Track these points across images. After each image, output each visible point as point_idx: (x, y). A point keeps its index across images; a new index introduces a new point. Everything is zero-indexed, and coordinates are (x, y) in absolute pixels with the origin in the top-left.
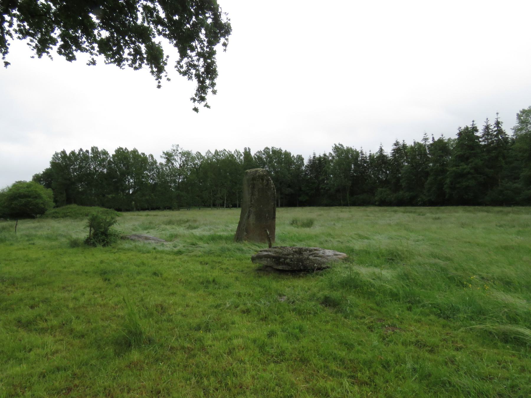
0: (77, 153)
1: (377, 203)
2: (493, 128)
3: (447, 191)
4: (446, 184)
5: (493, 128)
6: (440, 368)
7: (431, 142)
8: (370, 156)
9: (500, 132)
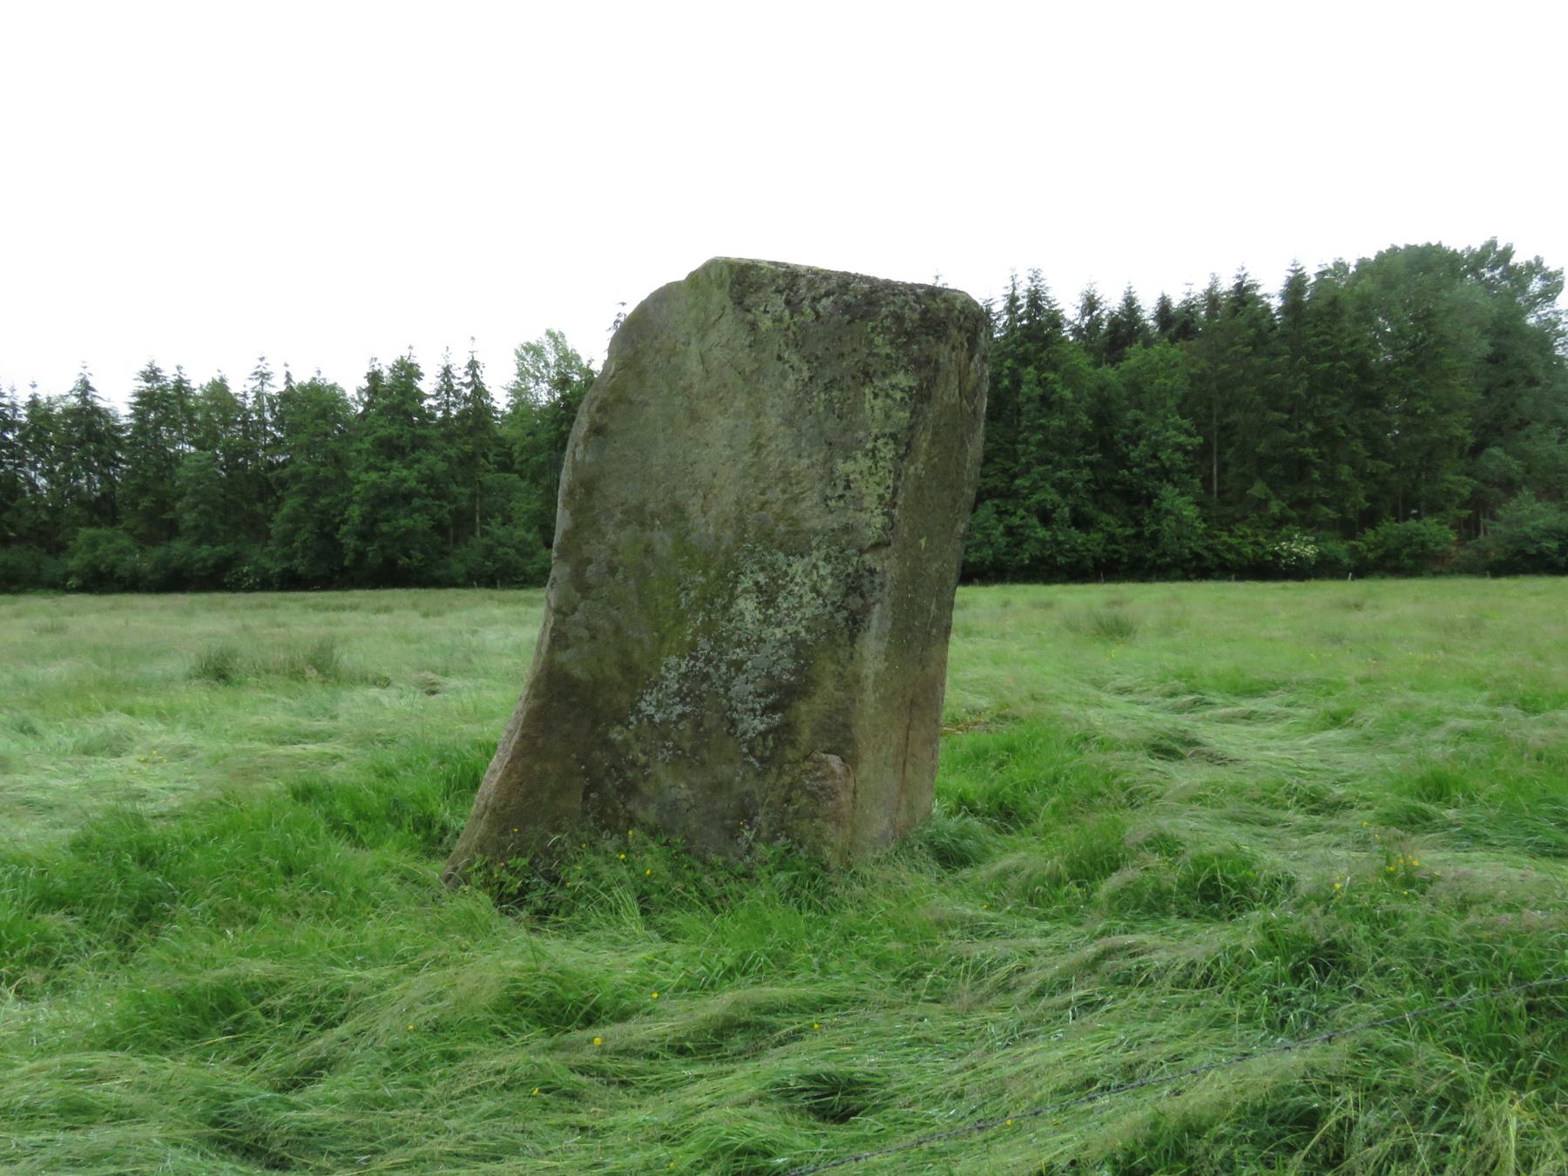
0: (1276, 303)
1: (73, 582)
2: (461, 375)
3: (352, 542)
4: (344, 522)
5: (461, 375)
6: (1515, 465)
7: (283, 388)
8: (34, 404)
9: (479, 391)
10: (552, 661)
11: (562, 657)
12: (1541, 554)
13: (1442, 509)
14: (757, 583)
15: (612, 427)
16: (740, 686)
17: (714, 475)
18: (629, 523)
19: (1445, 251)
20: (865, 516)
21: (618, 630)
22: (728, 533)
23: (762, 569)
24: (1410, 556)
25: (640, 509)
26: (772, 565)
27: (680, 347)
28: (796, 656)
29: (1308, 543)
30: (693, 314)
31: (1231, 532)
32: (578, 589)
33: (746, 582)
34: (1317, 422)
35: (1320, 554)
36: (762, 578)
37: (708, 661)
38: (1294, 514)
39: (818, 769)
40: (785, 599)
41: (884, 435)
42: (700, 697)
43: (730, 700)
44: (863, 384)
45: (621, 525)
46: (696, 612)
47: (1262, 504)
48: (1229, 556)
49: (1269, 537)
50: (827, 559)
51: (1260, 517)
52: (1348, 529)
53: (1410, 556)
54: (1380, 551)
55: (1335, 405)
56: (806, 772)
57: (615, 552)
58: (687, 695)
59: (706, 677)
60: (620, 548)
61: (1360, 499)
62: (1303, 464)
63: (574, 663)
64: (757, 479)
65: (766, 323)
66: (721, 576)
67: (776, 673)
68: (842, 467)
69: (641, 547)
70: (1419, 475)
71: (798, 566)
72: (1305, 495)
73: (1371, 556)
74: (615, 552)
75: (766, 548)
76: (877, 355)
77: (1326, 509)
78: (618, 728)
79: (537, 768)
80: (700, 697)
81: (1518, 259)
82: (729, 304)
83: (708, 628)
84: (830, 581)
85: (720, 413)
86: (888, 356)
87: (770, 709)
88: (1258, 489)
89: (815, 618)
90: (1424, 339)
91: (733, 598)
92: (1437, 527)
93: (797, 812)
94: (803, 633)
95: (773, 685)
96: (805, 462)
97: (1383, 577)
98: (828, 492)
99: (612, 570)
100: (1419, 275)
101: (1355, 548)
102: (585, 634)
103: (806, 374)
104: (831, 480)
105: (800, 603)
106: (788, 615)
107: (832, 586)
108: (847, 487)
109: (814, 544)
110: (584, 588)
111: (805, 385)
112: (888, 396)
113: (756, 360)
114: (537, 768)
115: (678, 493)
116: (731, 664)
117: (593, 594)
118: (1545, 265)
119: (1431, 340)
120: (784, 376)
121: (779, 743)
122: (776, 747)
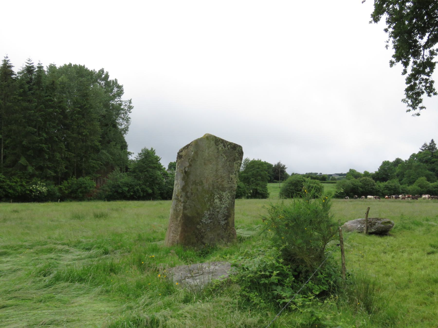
11: (186, 212)
12: (123, 193)
13: (90, 174)
16: (220, 216)
19: (87, 70)
20: (234, 185)
21: (195, 206)
24: (81, 192)
25: (195, 181)
28: (227, 210)
29: (43, 186)
30: (207, 145)
31: (10, 179)
33: (216, 197)
34: (47, 133)
35: (48, 191)
36: (218, 196)
37: (213, 211)
38: (37, 173)
45: (192, 185)
46: (208, 202)
47: (24, 168)
48: (11, 191)
49: (27, 182)
50: (229, 192)
51: (24, 173)
52: (58, 180)
53: (81, 192)
54: (70, 190)
59: (213, 214)
61: (62, 168)
62: (41, 151)
63: (188, 213)
65: (220, 149)
66: (211, 195)
68: (231, 176)
70: (82, 159)
71: (224, 194)
72: (42, 164)
73: (66, 192)
74: (192, 190)
77: (49, 171)
79: (186, 234)
81: (111, 78)
82: (214, 144)
83: (211, 205)
87: (225, 220)
88: (23, 161)
89: (229, 203)
90: (85, 105)
91: (214, 200)
95: (225, 215)
96: (225, 175)
97: (71, 201)
99: (192, 194)
100: (78, 75)
102: (189, 207)
103: (226, 159)
110: (188, 197)
114: (186, 234)
118: (118, 83)
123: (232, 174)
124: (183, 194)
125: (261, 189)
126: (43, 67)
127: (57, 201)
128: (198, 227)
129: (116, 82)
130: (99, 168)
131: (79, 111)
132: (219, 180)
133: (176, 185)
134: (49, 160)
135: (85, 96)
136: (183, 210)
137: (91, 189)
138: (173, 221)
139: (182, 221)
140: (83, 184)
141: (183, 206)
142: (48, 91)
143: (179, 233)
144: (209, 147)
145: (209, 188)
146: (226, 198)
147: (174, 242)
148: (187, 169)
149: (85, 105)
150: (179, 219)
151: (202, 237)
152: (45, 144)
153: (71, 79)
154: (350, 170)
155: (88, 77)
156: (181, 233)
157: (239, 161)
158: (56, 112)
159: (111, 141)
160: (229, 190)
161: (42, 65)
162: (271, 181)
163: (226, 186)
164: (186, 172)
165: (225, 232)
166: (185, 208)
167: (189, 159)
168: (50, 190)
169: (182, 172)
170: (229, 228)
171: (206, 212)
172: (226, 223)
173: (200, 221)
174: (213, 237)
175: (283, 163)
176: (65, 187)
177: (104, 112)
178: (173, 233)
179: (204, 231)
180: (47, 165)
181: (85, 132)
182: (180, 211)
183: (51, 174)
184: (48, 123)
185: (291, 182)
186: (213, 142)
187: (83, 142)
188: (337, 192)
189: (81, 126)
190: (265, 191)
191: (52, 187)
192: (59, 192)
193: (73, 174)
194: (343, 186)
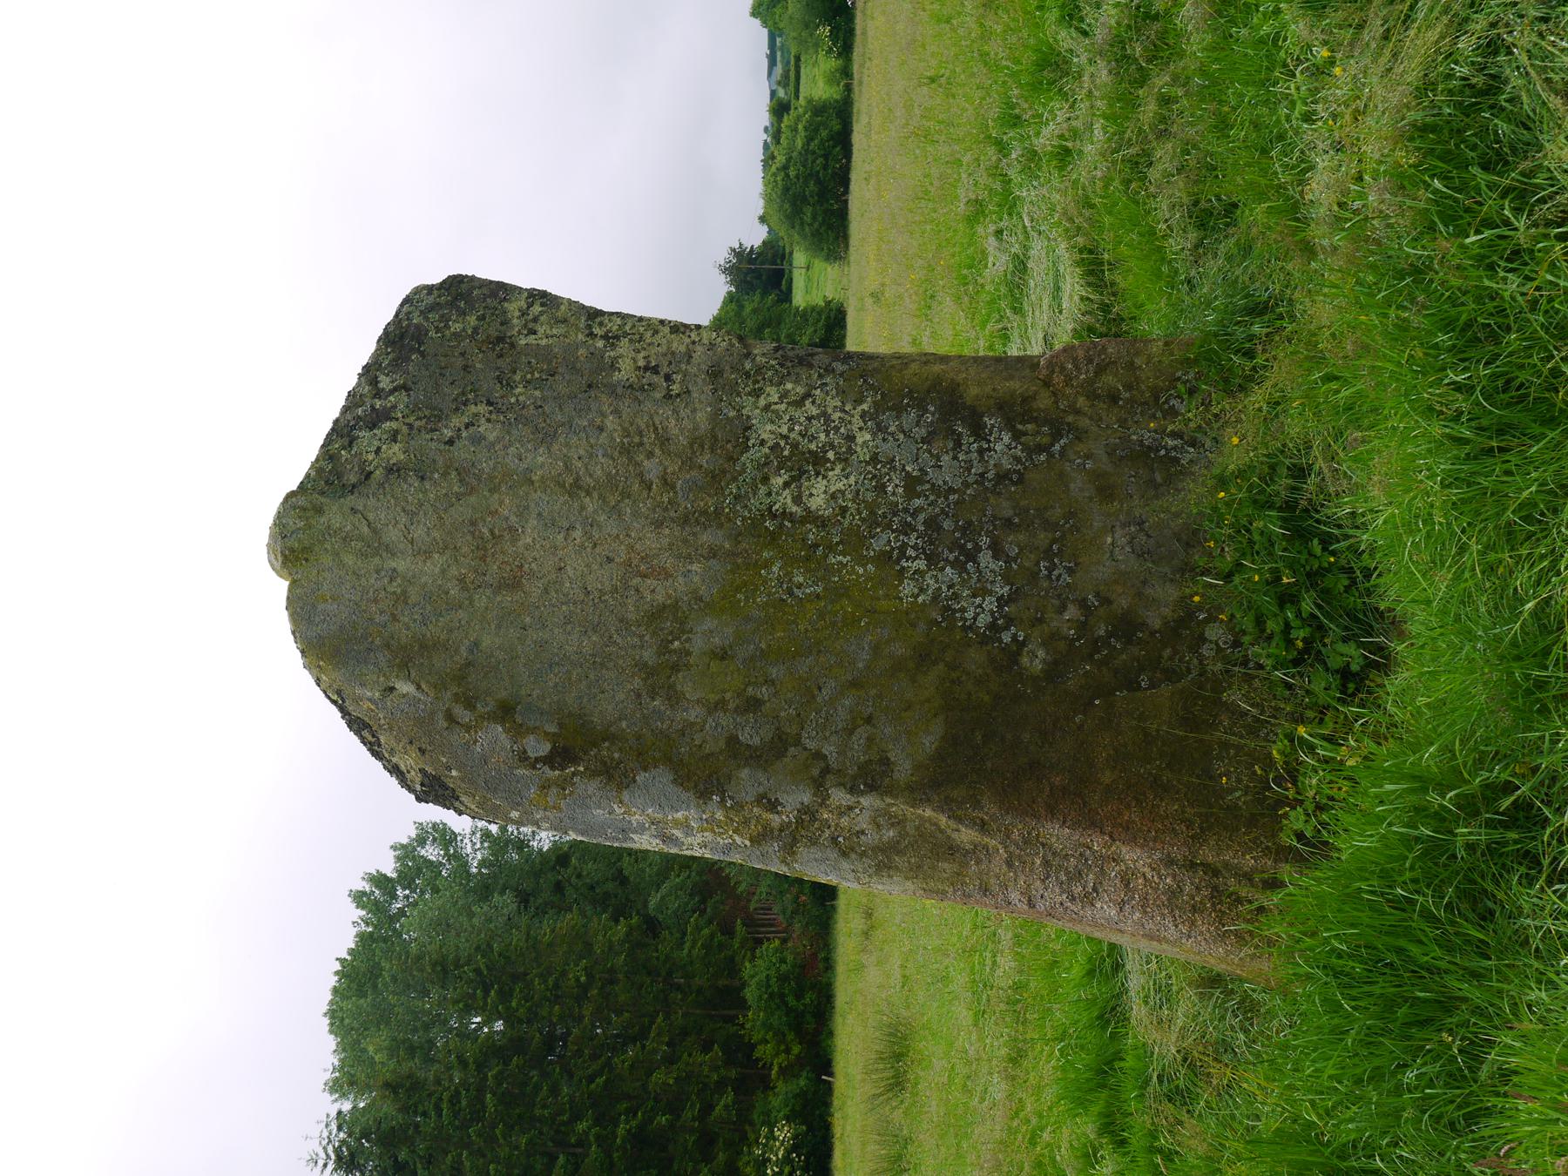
10: (911, 788)
11: (903, 769)
13: (732, 959)
14: (786, 485)
15: (503, 694)
16: (947, 473)
17: (610, 560)
18: (672, 687)
21: (855, 684)
22: (706, 538)
23: (765, 480)
24: (799, 997)
25: (648, 671)
26: (760, 467)
27: (394, 587)
28: (899, 410)
29: (771, 1136)
30: (349, 560)
32: (781, 754)
33: (785, 499)
34: (576, 1117)
36: (778, 481)
37: (906, 529)
39: (1063, 369)
40: (813, 438)
41: (589, 327)
42: (964, 530)
43: (966, 485)
44: (513, 346)
45: (674, 698)
46: (829, 570)
50: (757, 393)
53: (799, 997)
54: (790, 1036)
55: (555, 1091)
56: (1068, 380)
57: (720, 705)
58: (962, 548)
60: (713, 697)
61: (706, 1062)
62: (641, 1139)
64: (626, 495)
65: (395, 453)
67: (924, 432)
69: (715, 666)
70: (679, 988)
71: (766, 431)
73: (796, 1049)
74: (720, 705)
75: (735, 479)
76: (475, 329)
78: (1025, 660)
79: (1107, 777)
80: (964, 530)
81: (389, 868)
82: (351, 500)
83: (855, 542)
84: (789, 386)
85: (514, 541)
86: (482, 318)
87: (978, 431)
89: (841, 392)
90: (478, 971)
91: (810, 517)
92: (759, 962)
93: (1128, 387)
94: (865, 407)
95: (942, 431)
96: (610, 422)
97: (831, 1034)
98: (658, 395)
99: (753, 705)
101: (783, 1071)
102: (862, 732)
103: (482, 408)
104: (642, 389)
105: (817, 417)
106: (837, 429)
107: (797, 382)
108: (655, 370)
109: (732, 414)
110: (779, 745)
111: (499, 411)
112: (535, 320)
113: (445, 475)
115: (632, 616)
116: (911, 492)
117: (792, 730)
118: (405, 841)
119: (481, 961)
120: (478, 440)
121: (1028, 417)
122: (1035, 420)
123: (613, 366)
124: (747, 782)
125: (810, 330)
126: (340, 1113)
127: (829, 1088)
128: (1035, 660)
129: (403, 847)
130: (713, 927)
131: (501, 992)
132: (652, 468)
133: (666, 839)
134: (675, 1109)
135: (445, 971)
136: (890, 791)
137: (790, 958)
138: (985, 890)
139: (990, 809)
140: (768, 986)
141: (852, 790)
142: (420, 1109)
143: (1097, 843)
144: (376, 546)
145: (713, 553)
146: (799, 415)
147: (1173, 894)
148: (538, 747)
149: (478, 971)
150: (966, 836)
151: (1127, 627)
152: (616, 1125)
153: (382, 1017)
154: (753, 14)
155: (377, 952)
156: (1092, 822)
157: (514, 308)
158: (499, 1079)
159: (620, 871)
160: (733, 390)
161: (333, 1114)
162: (787, 296)
163: (702, 417)
164: (561, 756)
165: (1080, 435)
166: (872, 777)
167: (450, 717)
168: (786, 1111)
169: (563, 784)
170: (1044, 401)
171: (908, 588)
172: (1009, 425)
173: (984, 640)
174: (1121, 537)
175: (723, 256)
176: (777, 1054)
177: (506, 902)
178: (1088, 899)
179: (1072, 612)
180: (694, 1119)
181: (577, 973)
182: (899, 822)
183: (726, 1107)
184: (537, 1112)
185: (787, 217)
186: (335, 515)
187: (612, 982)
188: (830, 50)
189: (556, 986)
190: (819, 314)
191: (775, 1102)
192: (797, 1076)
193: (731, 1020)
194: (807, 26)
